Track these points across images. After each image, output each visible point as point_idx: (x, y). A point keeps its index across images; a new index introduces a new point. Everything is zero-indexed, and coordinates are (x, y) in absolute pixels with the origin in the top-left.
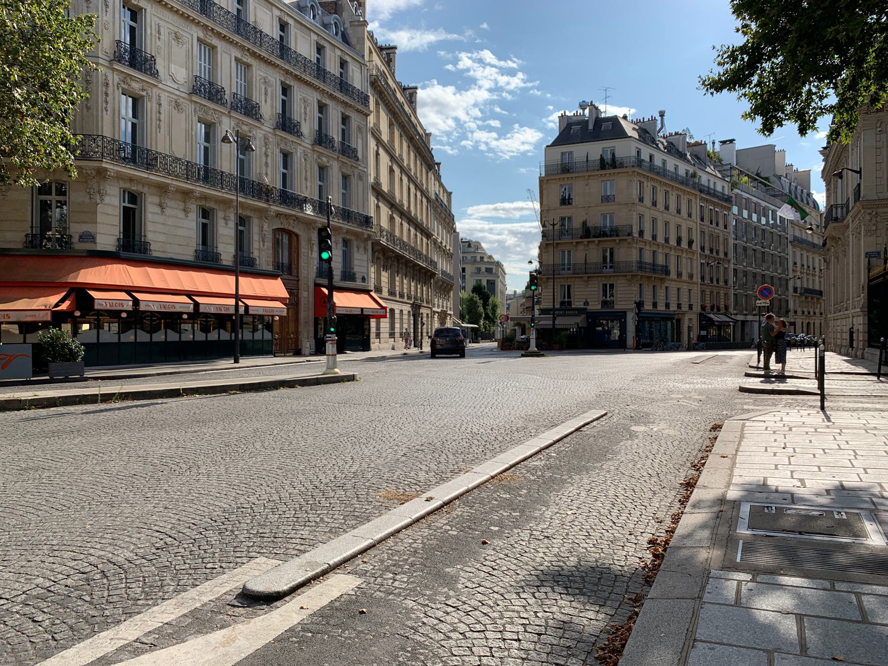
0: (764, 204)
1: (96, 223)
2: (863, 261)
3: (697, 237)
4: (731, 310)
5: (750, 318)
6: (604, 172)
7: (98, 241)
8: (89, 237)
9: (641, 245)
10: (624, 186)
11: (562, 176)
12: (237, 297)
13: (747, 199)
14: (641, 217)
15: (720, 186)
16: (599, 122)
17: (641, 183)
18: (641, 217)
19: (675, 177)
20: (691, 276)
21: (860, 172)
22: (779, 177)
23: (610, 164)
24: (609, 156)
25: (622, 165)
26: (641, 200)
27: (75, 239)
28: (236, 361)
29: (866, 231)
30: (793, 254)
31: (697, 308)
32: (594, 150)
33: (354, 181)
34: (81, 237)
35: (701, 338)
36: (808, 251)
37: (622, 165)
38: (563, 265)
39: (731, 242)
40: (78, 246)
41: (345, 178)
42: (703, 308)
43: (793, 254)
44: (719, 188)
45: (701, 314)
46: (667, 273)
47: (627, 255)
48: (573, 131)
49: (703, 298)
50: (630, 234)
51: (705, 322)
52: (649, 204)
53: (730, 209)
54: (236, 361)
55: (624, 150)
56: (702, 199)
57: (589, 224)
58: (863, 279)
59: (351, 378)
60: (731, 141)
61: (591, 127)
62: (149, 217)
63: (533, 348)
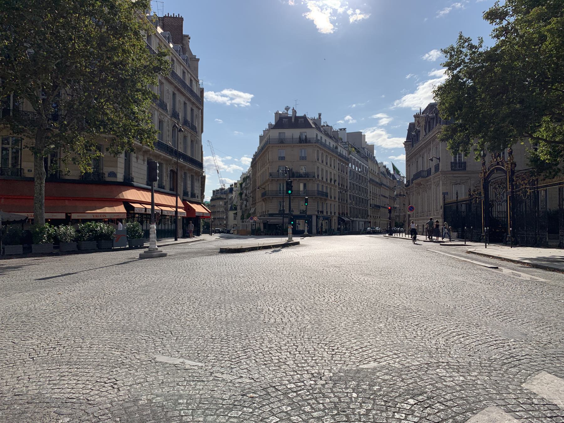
0: (360, 162)
1: (457, 202)
2: (441, 196)
3: (337, 178)
4: (349, 215)
5: (355, 219)
6: (301, 145)
7: (118, 177)
8: (114, 174)
9: (318, 182)
10: (310, 152)
11: (279, 145)
12: (152, 203)
13: (354, 160)
14: (318, 168)
15: (345, 153)
16: (297, 118)
17: (318, 151)
18: (318, 168)
19: (329, 148)
20: (335, 198)
21: (439, 159)
22: (364, 148)
23: (303, 141)
24: (304, 137)
25: (310, 142)
26: (318, 160)
27: (106, 175)
28: (176, 240)
29: (443, 184)
30: (371, 188)
31: (337, 215)
32: (295, 133)
33: (194, 143)
34: (109, 174)
35: (339, 229)
36: (375, 186)
37: (310, 142)
38: (280, 191)
39: (349, 181)
40: (108, 179)
41: (192, 141)
42: (339, 214)
43: (371, 188)
44: (344, 154)
45: (339, 217)
46: (327, 196)
47: (313, 187)
48: (284, 122)
49: (339, 210)
50: (314, 177)
51: (340, 220)
52: (325, 164)
53: (348, 165)
54: (176, 240)
55: (311, 133)
56: (340, 160)
57: (294, 170)
58: (442, 204)
59: (298, 243)
60: (345, 129)
61: (293, 120)
62: (133, 163)
63: (306, 233)
